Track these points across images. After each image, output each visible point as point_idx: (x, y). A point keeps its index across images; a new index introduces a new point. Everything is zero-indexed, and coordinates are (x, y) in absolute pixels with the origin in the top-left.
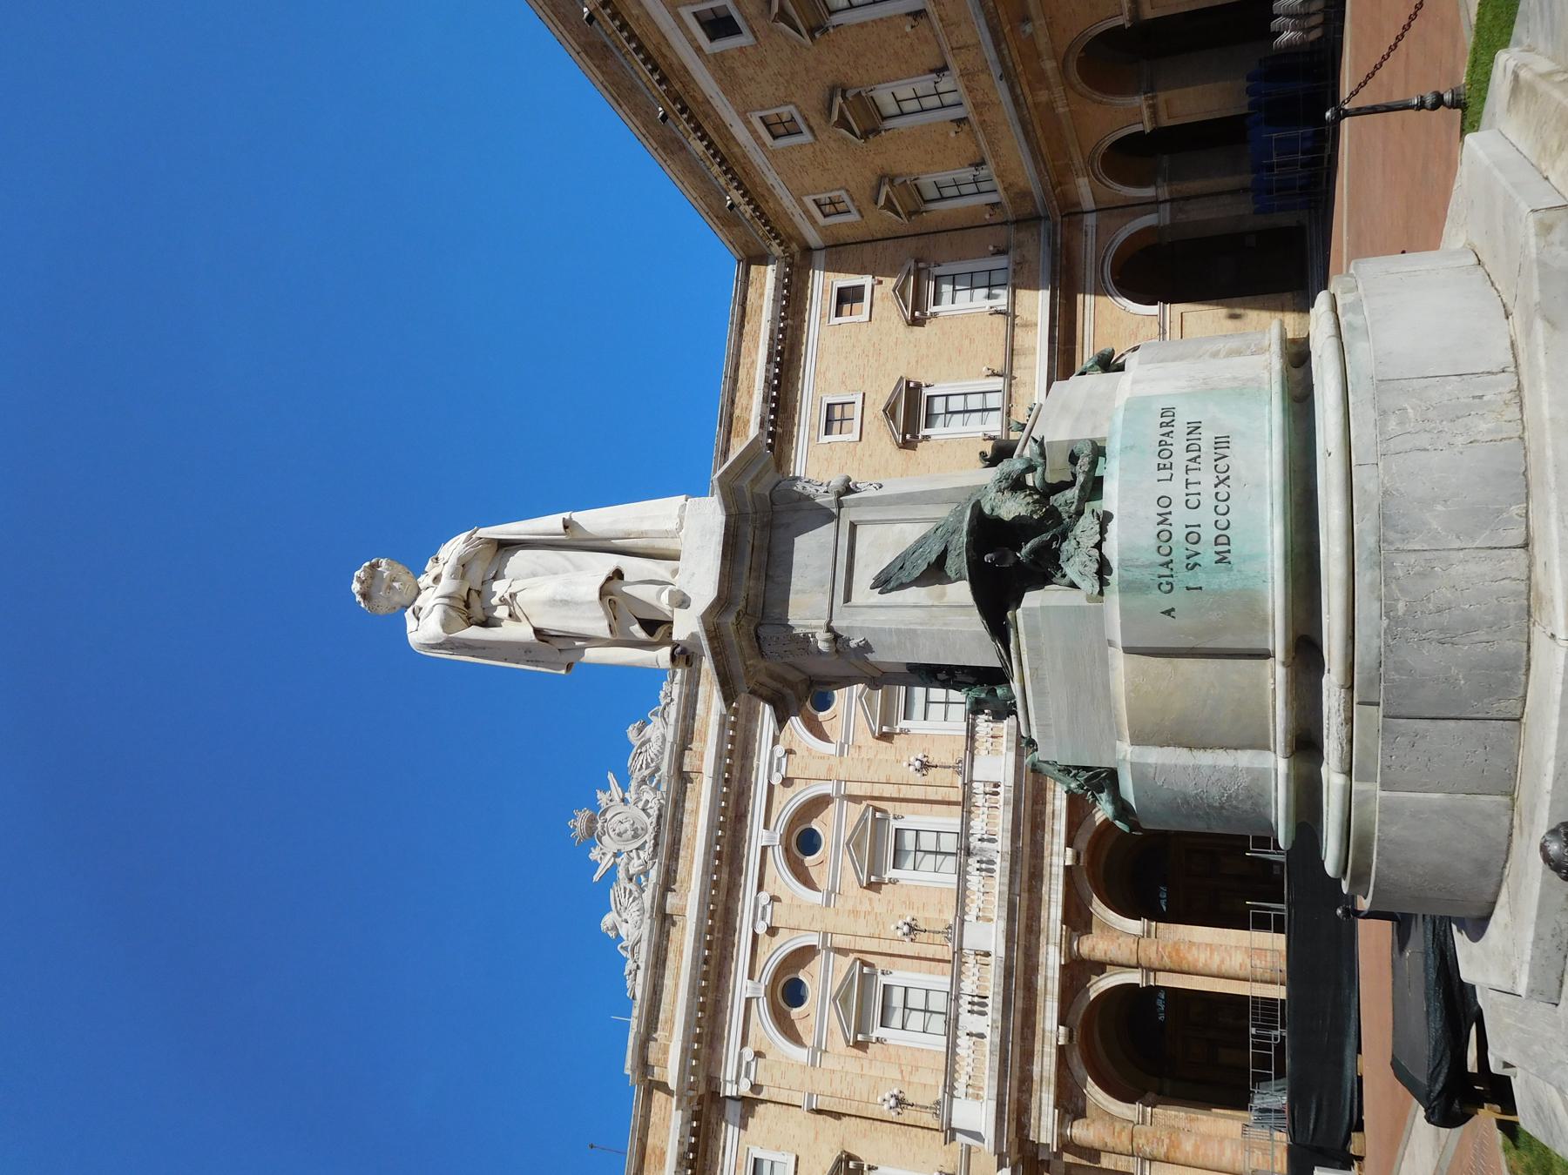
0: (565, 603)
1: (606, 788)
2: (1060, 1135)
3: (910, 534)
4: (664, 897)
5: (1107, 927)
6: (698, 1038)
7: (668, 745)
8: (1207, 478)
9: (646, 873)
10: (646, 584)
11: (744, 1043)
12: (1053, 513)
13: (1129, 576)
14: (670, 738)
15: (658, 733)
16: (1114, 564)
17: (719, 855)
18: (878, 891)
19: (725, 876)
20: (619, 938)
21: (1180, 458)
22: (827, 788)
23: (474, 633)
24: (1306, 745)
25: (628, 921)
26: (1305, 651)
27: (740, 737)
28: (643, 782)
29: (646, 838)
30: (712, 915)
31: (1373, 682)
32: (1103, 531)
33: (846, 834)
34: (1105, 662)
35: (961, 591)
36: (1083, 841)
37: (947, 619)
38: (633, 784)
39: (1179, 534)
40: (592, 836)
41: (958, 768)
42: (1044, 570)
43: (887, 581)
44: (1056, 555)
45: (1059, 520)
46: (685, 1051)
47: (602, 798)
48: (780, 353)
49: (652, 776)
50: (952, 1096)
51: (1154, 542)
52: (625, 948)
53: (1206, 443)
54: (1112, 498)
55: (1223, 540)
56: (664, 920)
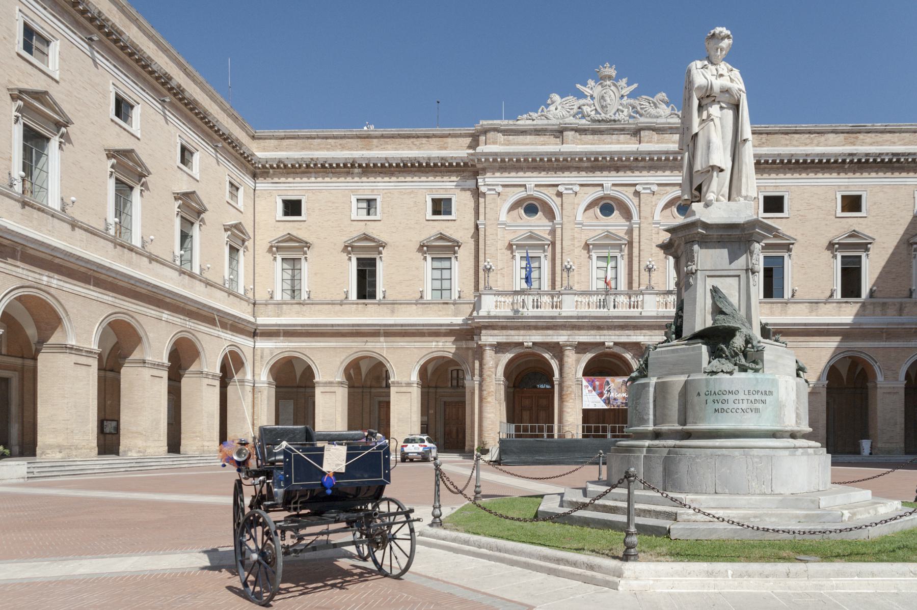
0: (709, 148)
1: (629, 84)
2: (485, 345)
3: (734, 299)
4: (572, 130)
5: (578, 361)
6: (503, 161)
7: (655, 120)
8: (745, 406)
9: (583, 117)
10: (717, 186)
11: (504, 186)
12: (736, 354)
13: (711, 382)
14: (659, 121)
15: (662, 113)
16: (714, 377)
17: (596, 160)
18: (584, 248)
19: (586, 165)
20: (547, 106)
21: (752, 398)
22: (635, 218)
23: (696, 102)
24: (657, 435)
25: (559, 109)
26: (688, 435)
27: (662, 163)
28: (633, 107)
29: (603, 115)
30: (565, 160)
31: (676, 453)
32: (727, 373)
33: (612, 229)
34: (682, 373)
35: (709, 323)
36: (617, 350)
37: (701, 318)
38: (632, 101)
39: (725, 397)
40: (600, 79)
41: (650, 287)
42: (715, 353)
43: (715, 292)
44: (721, 357)
45: (733, 357)
46: (496, 154)
47: (623, 82)
48: (898, 161)
49: (637, 112)
50: (495, 295)
51: (723, 389)
52: (542, 111)
53: (757, 405)
54: (738, 375)
55: (723, 411)
56: (559, 132)
